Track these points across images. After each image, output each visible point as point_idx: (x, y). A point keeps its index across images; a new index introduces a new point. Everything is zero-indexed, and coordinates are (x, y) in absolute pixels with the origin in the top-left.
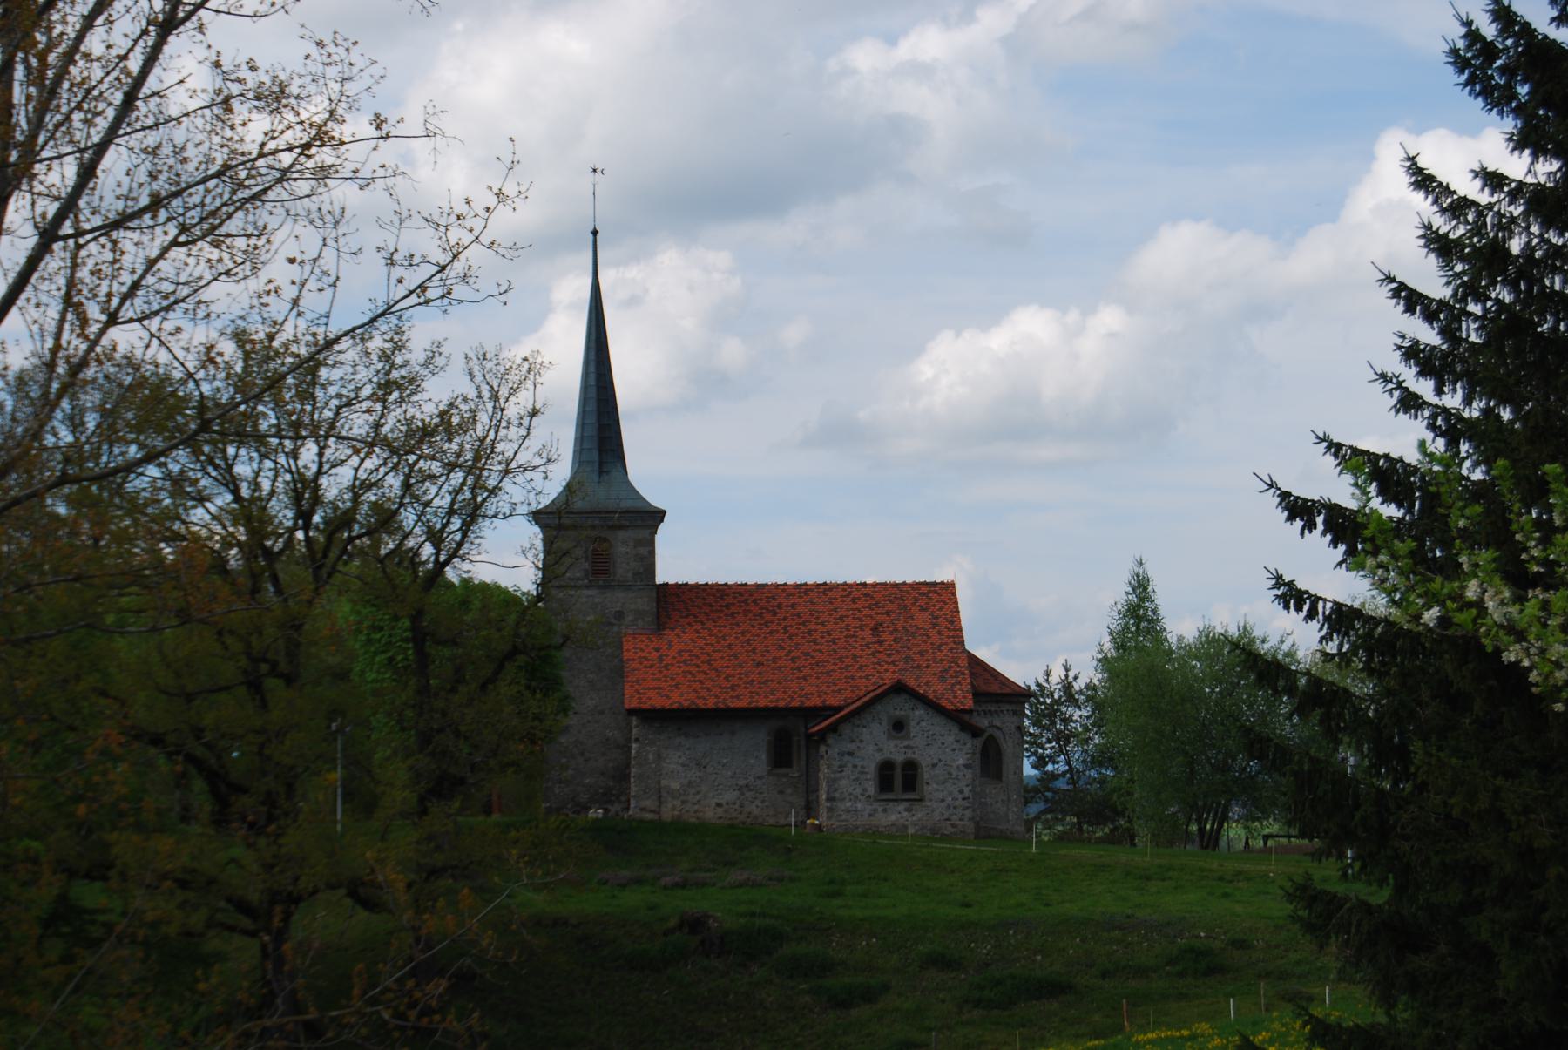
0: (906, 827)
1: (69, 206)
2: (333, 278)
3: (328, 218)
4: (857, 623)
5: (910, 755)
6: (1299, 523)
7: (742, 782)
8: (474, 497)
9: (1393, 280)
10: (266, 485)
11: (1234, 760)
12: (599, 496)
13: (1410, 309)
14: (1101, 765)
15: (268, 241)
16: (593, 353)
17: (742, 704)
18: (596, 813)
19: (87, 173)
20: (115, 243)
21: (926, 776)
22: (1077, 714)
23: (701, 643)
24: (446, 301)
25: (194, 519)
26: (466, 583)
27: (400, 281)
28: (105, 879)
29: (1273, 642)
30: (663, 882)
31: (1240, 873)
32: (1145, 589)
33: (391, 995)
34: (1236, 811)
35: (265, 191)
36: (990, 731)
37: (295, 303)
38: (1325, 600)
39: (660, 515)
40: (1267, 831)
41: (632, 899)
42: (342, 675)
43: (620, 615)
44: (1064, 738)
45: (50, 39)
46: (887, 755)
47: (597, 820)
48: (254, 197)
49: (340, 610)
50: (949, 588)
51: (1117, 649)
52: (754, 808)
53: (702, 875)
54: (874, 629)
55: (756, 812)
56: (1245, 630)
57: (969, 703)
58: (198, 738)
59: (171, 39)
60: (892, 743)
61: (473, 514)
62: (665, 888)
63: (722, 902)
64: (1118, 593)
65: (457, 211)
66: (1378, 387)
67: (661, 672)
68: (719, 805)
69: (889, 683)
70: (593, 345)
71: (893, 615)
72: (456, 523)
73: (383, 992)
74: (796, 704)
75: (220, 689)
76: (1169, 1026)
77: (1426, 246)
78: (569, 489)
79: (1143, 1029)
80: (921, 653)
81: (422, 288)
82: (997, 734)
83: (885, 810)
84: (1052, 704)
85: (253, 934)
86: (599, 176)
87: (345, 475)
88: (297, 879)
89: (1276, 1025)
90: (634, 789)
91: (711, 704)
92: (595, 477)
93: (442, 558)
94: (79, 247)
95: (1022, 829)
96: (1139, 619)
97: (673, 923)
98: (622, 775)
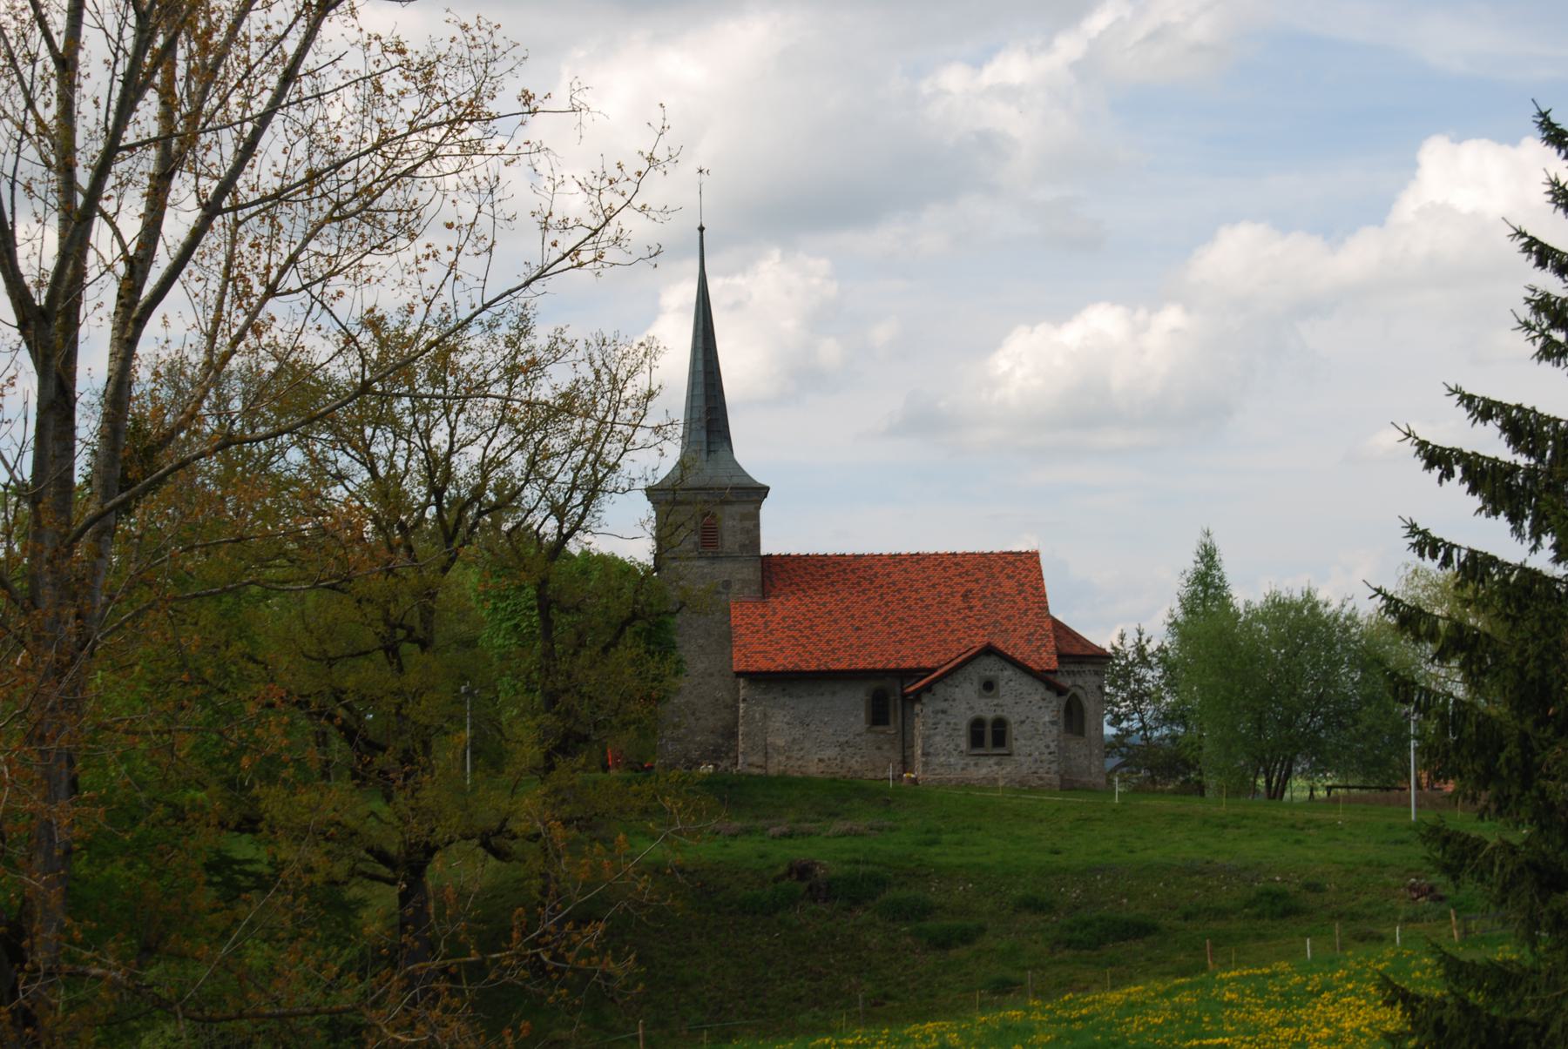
0: (996, 780)
1: (227, 185)
2: (489, 243)
3: (484, 184)
4: (948, 590)
5: (999, 713)
6: (1437, 471)
7: (843, 739)
8: (595, 473)
9: (1524, 235)
10: (401, 464)
11: (1298, 716)
12: (708, 473)
13: (1541, 263)
14: (1172, 721)
15: (418, 217)
16: (700, 340)
17: (843, 666)
18: (707, 769)
19: (247, 150)
20: (273, 218)
21: (1015, 732)
22: (1149, 675)
23: (803, 609)
24: (598, 264)
25: (334, 496)
26: (586, 554)
27: (555, 245)
28: (254, 831)
29: (1335, 606)
30: (771, 832)
31: (1309, 821)
32: (1212, 558)
33: (550, 938)
34: (1301, 765)
35: (415, 167)
36: (1073, 690)
37: (453, 265)
38: (1459, 548)
39: (763, 491)
40: (1329, 783)
41: (743, 848)
42: (470, 643)
43: (727, 584)
44: (1138, 697)
45: (209, 23)
46: (978, 713)
47: (710, 775)
48: (405, 174)
49: (467, 580)
50: (1033, 557)
51: (1186, 613)
52: (855, 763)
53: (807, 825)
54: (965, 596)
55: (856, 767)
56: (1308, 596)
57: (1054, 665)
58: (339, 700)
59: (325, 24)
60: (983, 702)
61: (593, 490)
62: (773, 837)
63: (829, 847)
64: (1189, 562)
65: (609, 176)
66: (1522, 335)
67: (769, 634)
68: (820, 760)
69: (979, 646)
70: (700, 333)
71: (982, 583)
72: (578, 497)
73: (542, 935)
74: (892, 665)
75: (360, 654)
76: (1250, 965)
77: (1554, 201)
78: (682, 464)
79: (1225, 967)
80: (1008, 618)
81: (575, 251)
82: (1080, 692)
83: (976, 765)
84: (1126, 666)
85: (392, 882)
86: (704, 175)
87: (475, 453)
88: (433, 830)
89: (1352, 963)
90: (741, 746)
91: (813, 667)
92: (704, 456)
93: (565, 531)
94: (238, 223)
95: (1103, 781)
96: (1207, 586)
97: (782, 870)
98: (731, 733)
